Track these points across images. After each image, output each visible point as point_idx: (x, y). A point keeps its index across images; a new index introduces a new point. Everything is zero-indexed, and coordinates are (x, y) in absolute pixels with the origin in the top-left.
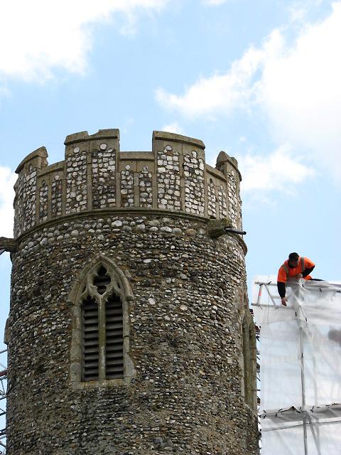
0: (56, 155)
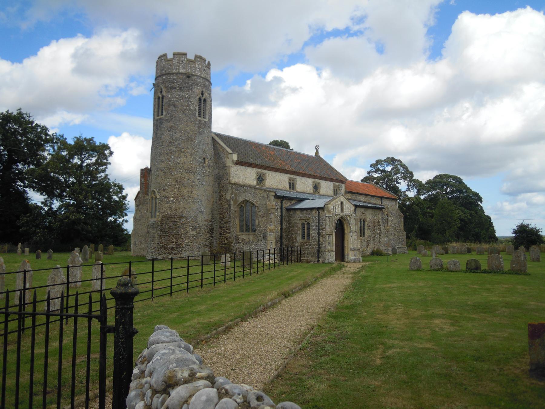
0: (170, 56)
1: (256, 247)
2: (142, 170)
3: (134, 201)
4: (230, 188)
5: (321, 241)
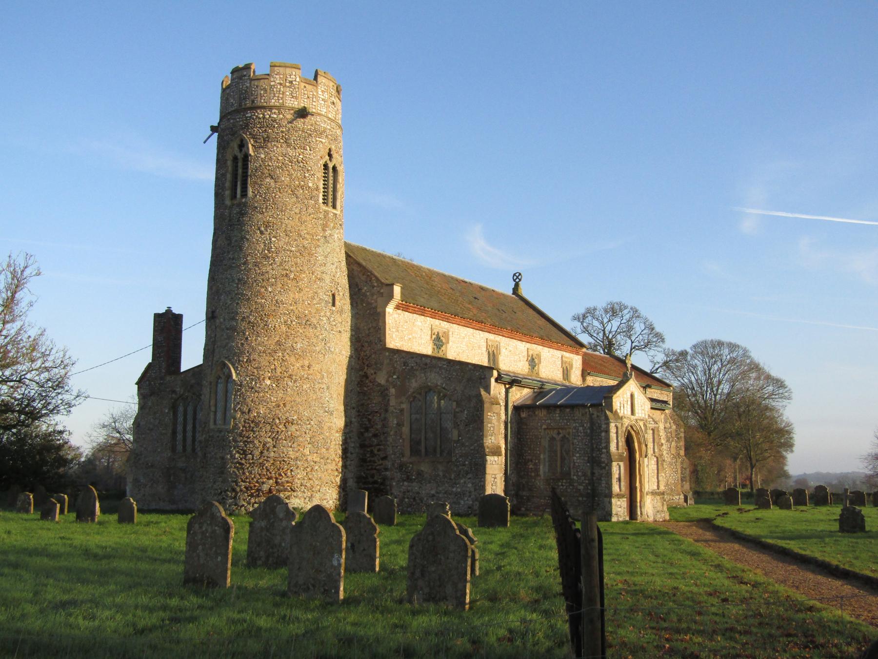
1: (454, 489)
2: (157, 316)
3: (137, 386)
4: (386, 362)
5: (597, 474)
